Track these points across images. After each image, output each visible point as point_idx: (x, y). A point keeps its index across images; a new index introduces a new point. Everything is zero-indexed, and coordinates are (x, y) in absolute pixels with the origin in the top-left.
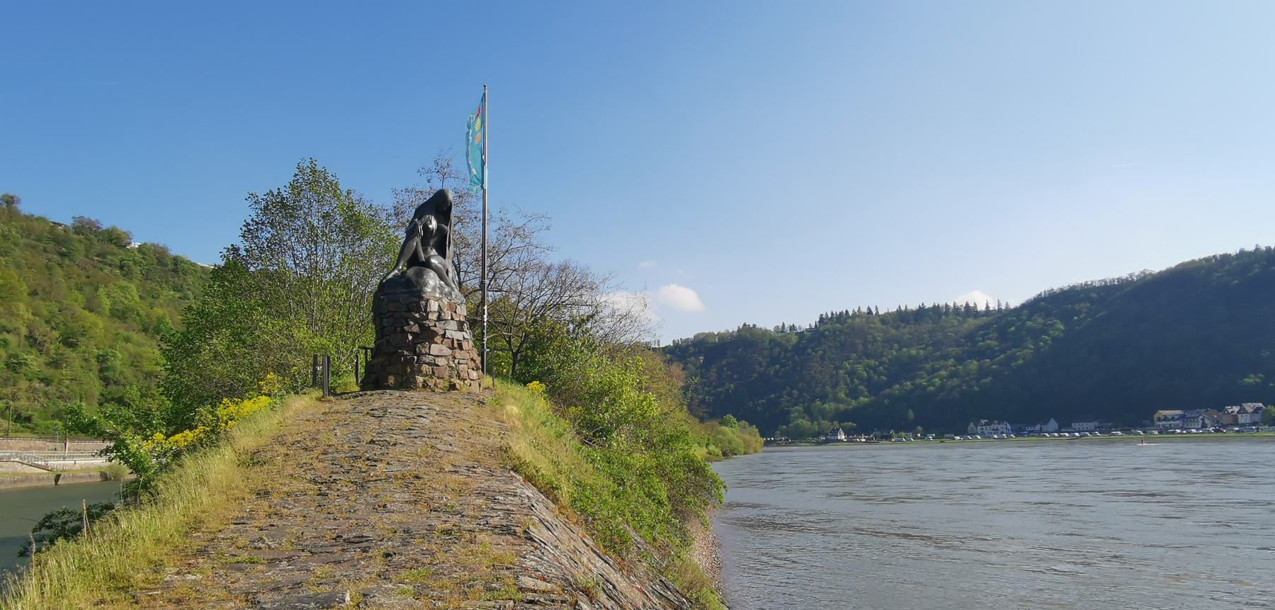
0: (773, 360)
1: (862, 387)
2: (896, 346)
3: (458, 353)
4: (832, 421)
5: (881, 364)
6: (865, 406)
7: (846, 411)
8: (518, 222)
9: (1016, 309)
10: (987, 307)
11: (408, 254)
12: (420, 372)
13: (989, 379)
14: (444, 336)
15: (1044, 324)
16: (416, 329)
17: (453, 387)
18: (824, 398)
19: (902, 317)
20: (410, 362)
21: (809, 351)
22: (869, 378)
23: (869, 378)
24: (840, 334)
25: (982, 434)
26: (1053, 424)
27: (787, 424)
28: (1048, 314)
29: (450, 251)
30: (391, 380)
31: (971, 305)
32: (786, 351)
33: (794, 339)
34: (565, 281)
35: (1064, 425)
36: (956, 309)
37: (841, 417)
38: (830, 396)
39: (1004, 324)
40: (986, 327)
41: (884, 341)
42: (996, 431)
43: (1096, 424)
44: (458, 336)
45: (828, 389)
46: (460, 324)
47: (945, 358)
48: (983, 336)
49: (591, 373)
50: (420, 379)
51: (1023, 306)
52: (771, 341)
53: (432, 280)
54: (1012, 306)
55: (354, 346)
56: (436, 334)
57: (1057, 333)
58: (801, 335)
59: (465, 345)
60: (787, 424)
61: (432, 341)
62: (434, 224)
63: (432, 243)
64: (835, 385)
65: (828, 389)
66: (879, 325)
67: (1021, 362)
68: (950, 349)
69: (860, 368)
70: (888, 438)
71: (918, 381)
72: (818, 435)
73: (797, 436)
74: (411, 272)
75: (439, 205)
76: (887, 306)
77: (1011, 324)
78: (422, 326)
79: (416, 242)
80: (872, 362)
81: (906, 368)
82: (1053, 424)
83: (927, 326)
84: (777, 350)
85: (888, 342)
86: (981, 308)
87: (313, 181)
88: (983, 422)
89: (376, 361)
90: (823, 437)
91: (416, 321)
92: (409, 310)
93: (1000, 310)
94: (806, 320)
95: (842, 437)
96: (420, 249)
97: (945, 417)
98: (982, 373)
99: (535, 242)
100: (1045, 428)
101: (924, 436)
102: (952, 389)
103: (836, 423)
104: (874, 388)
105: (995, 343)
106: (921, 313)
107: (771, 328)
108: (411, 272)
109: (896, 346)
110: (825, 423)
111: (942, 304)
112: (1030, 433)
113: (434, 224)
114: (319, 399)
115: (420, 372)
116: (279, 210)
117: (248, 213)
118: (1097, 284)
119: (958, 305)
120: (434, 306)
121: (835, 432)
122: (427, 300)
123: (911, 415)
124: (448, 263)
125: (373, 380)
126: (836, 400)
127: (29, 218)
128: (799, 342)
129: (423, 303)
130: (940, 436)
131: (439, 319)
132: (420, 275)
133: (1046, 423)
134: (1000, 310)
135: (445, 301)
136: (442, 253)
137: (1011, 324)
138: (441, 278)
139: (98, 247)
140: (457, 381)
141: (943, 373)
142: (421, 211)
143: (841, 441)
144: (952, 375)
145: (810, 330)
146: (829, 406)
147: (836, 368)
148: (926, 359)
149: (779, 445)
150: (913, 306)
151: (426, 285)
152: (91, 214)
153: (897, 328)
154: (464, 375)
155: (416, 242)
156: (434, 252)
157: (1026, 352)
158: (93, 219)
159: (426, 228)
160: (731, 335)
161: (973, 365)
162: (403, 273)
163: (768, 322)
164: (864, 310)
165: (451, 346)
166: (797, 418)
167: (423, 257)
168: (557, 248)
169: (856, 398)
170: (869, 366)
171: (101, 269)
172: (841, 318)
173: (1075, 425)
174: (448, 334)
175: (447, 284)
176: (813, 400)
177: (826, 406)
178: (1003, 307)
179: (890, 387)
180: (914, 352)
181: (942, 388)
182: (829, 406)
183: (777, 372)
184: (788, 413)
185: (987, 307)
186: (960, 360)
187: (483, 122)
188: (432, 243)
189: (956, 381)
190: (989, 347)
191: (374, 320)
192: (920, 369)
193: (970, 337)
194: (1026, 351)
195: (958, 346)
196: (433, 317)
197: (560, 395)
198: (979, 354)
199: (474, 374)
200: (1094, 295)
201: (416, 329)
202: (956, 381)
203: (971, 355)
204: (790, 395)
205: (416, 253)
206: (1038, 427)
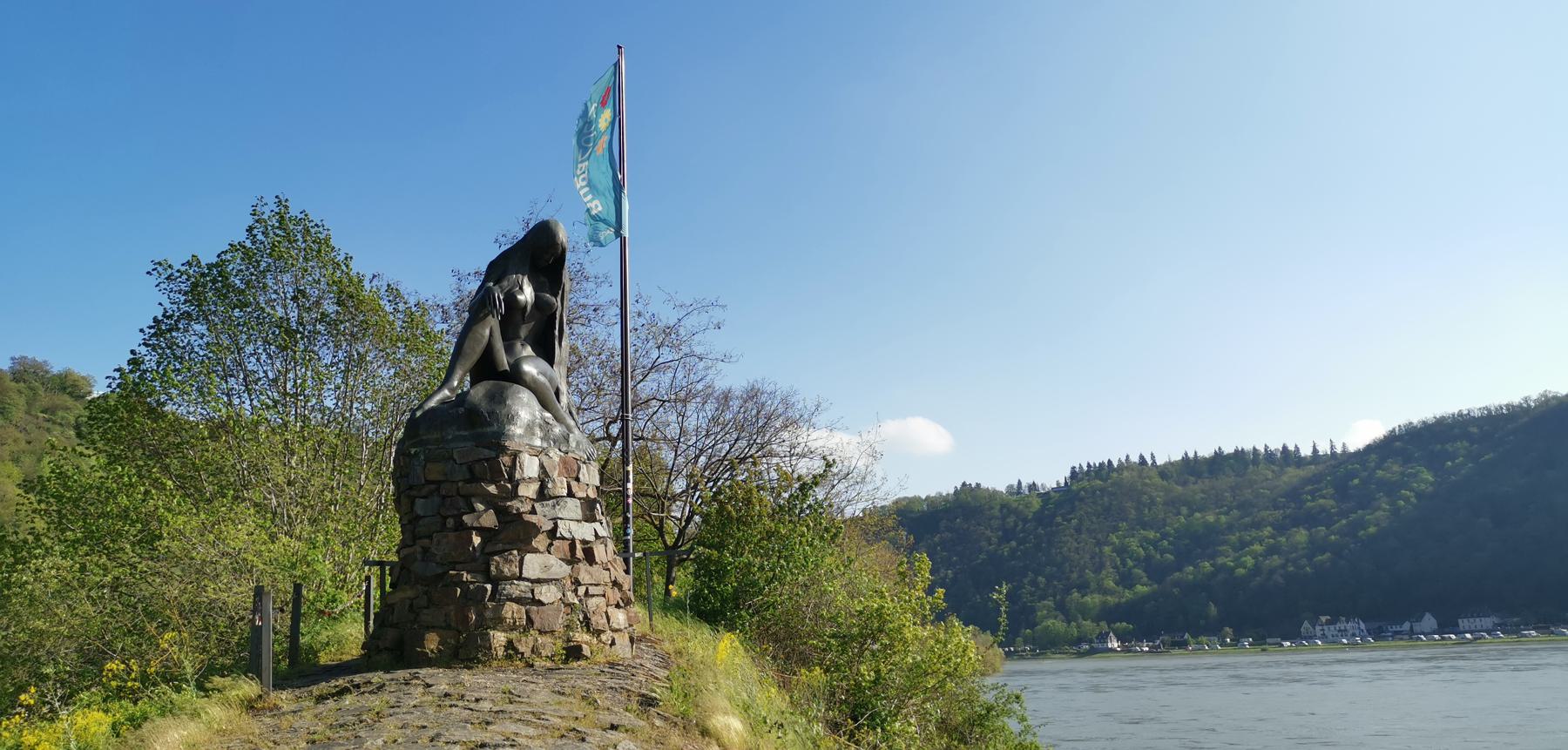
0: (1007, 536)
1: (1138, 571)
2: (1184, 510)
3: (585, 573)
4: (1097, 620)
5: (1165, 536)
6: (1145, 599)
7: (1118, 605)
8: (668, 317)
9: (1358, 453)
10: (1315, 450)
11: (474, 353)
12: (498, 622)
13: (1328, 555)
14: (552, 534)
15: (1402, 474)
16: (489, 519)
17: (574, 653)
18: (1083, 588)
19: (1190, 467)
20: (475, 598)
21: (1059, 519)
22: (1148, 558)
23: (1148, 558)
24: (1100, 493)
25: (1323, 637)
26: (1429, 621)
27: (1033, 626)
28: (1407, 459)
29: (562, 352)
30: (432, 643)
31: (1292, 448)
32: (1025, 521)
33: (1036, 504)
34: (757, 418)
35: (1447, 625)
36: (1269, 455)
37: (1110, 615)
38: (1093, 585)
39: (1342, 474)
40: (1316, 479)
41: (1166, 504)
42: (1343, 633)
43: (1496, 620)
44: (584, 531)
45: (1089, 574)
46: (589, 506)
47: (1258, 525)
48: (1312, 493)
49: (836, 590)
50: (499, 638)
51: (1369, 449)
52: (1003, 506)
53: (525, 408)
54: (1352, 449)
55: (344, 567)
56: (534, 530)
57: (1423, 486)
58: (1046, 496)
59: (599, 552)
60: (1033, 626)
61: (525, 546)
62: (527, 294)
63: (523, 332)
64: (1099, 568)
65: (1089, 574)
66: (1158, 480)
67: (1372, 530)
68: (1265, 513)
69: (1134, 544)
70: (1183, 645)
71: (1220, 560)
72: (1079, 640)
73: (1047, 645)
74: (479, 393)
75: (539, 253)
76: (1167, 452)
77: (1353, 475)
78: (502, 513)
79: (490, 327)
80: (1151, 534)
81: (1199, 543)
82: (1429, 621)
83: (1226, 481)
84: (1011, 520)
85: (1173, 504)
86: (1306, 451)
87: (283, 238)
88: (1323, 619)
89: (400, 595)
90: (1084, 646)
91: (490, 501)
92: (474, 478)
93: (1334, 454)
94: (1052, 476)
95: (1114, 644)
96: (499, 345)
97: (1266, 613)
98: (1316, 547)
99: (698, 350)
100: (1417, 628)
101: (1236, 642)
102: (1272, 571)
103: (1103, 624)
104: (1156, 572)
105: (1332, 502)
106: (1218, 461)
107: (1002, 488)
108: (479, 393)
109: (1184, 510)
110: (1088, 624)
111: (1248, 447)
112: (1396, 635)
113: (527, 294)
114: (251, 706)
115: (498, 622)
116: (206, 289)
117: (151, 302)
118: (1477, 414)
119: (1272, 448)
120: (530, 467)
121: (1103, 637)
122: (515, 456)
123: (1213, 610)
124: (559, 373)
125: (392, 647)
126: (1105, 591)
127: (59, 376)
128: (1043, 507)
129: (506, 460)
130: (1260, 641)
131: (542, 495)
132: (498, 398)
133: (1419, 619)
134: (1334, 454)
135: (555, 455)
136: (550, 358)
137: (1353, 475)
138: (545, 405)
139: (45, 399)
140: (581, 637)
141: (1257, 547)
142: (498, 269)
143: (1113, 650)
144: (1272, 551)
145: (1058, 489)
146: (1093, 600)
147: (1099, 544)
148: (1230, 528)
149: (1022, 658)
150: (1206, 452)
151: (511, 419)
152: (36, 352)
153: (1184, 484)
154: (598, 621)
155: (490, 327)
156: (528, 351)
157: (1379, 515)
158: (39, 359)
159: (511, 299)
160: (946, 499)
161: (1301, 536)
162: (462, 398)
163: (997, 480)
164: (1135, 459)
165: (567, 567)
166: (1046, 617)
167: (504, 361)
168: (739, 361)
169: (1131, 587)
170: (1146, 539)
171: (48, 430)
172: (1102, 471)
173: (1463, 623)
174: (563, 529)
175: (557, 418)
176: (1067, 591)
177: (1088, 599)
178: (1339, 450)
179: (1180, 569)
180: (1211, 518)
181: (1256, 570)
182: (1093, 600)
183: (1013, 551)
184: (1033, 610)
185: (1315, 450)
186: (1280, 528)
187: (617, 114)
188: (523, 332)
189: (1276, 560)
190: (1323, 509)
191: (397, 502)
192: (1225, 542)
193: (1294, 494)
194: (1379, 514)
195: (1276, 508)
196: (528, 491)
197: (785, 646)
198: (1310, 520)
199: (620, 618)
200: (1474, 430)
201: (489, 519)
202: (1276, 560)
203: (1296, 522)
204: (1034, 583)
205: (489, 350)
206: (1406, 626)
